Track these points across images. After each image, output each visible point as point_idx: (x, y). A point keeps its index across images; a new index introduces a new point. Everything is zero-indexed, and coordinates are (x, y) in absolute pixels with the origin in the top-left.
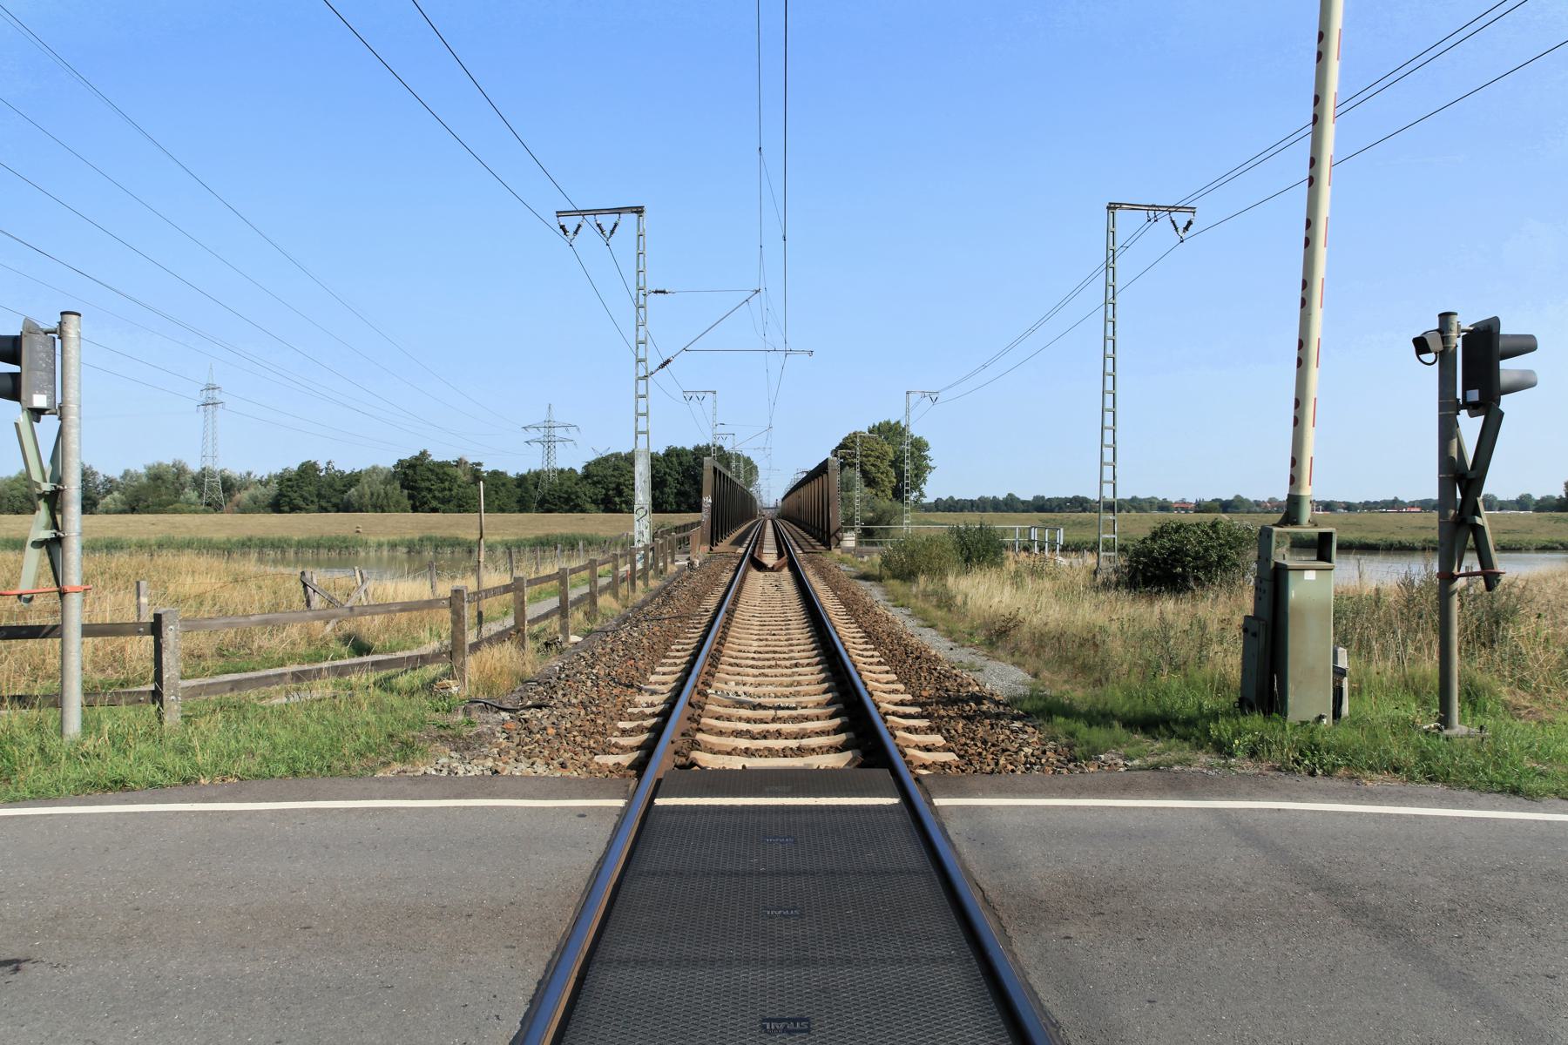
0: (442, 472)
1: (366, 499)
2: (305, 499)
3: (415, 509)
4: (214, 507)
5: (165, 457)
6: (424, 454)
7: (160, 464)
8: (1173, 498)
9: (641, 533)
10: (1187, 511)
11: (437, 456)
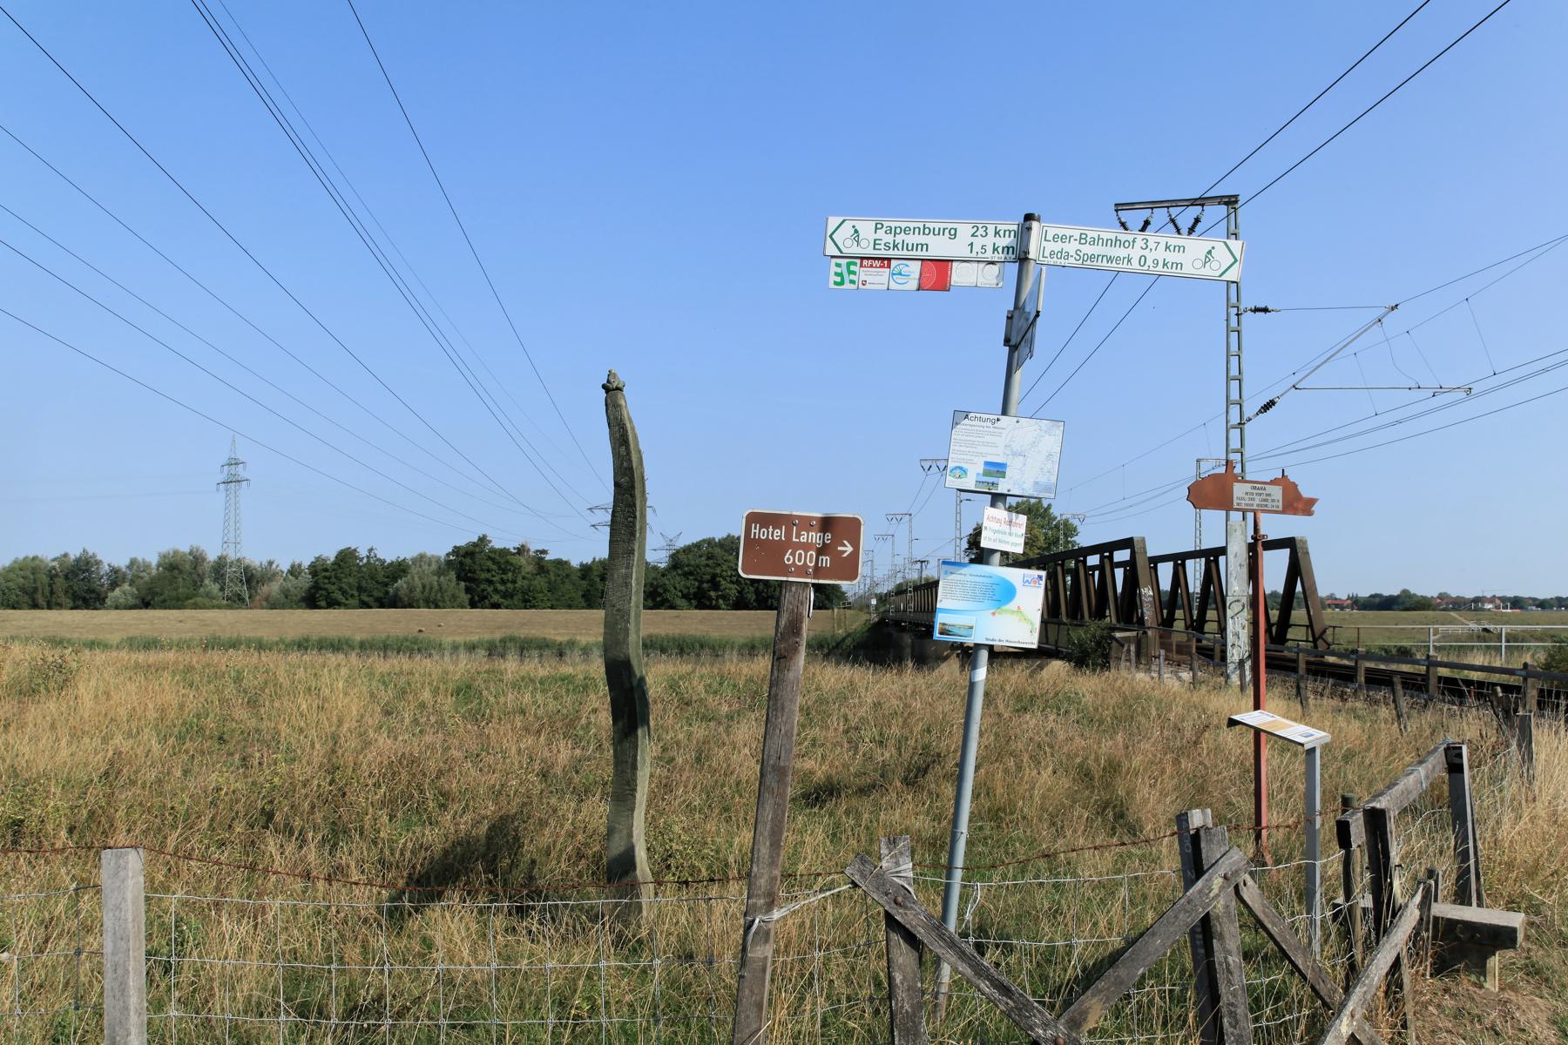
0: (503, 561)
1: (417, 594)
2: (344, 593)
3: (473, 605)
4: (236, 601)
5: (183, 545)
6: (483, 539)
7: (176, 552)
9: (1237, 635)
10: (1342, 608)
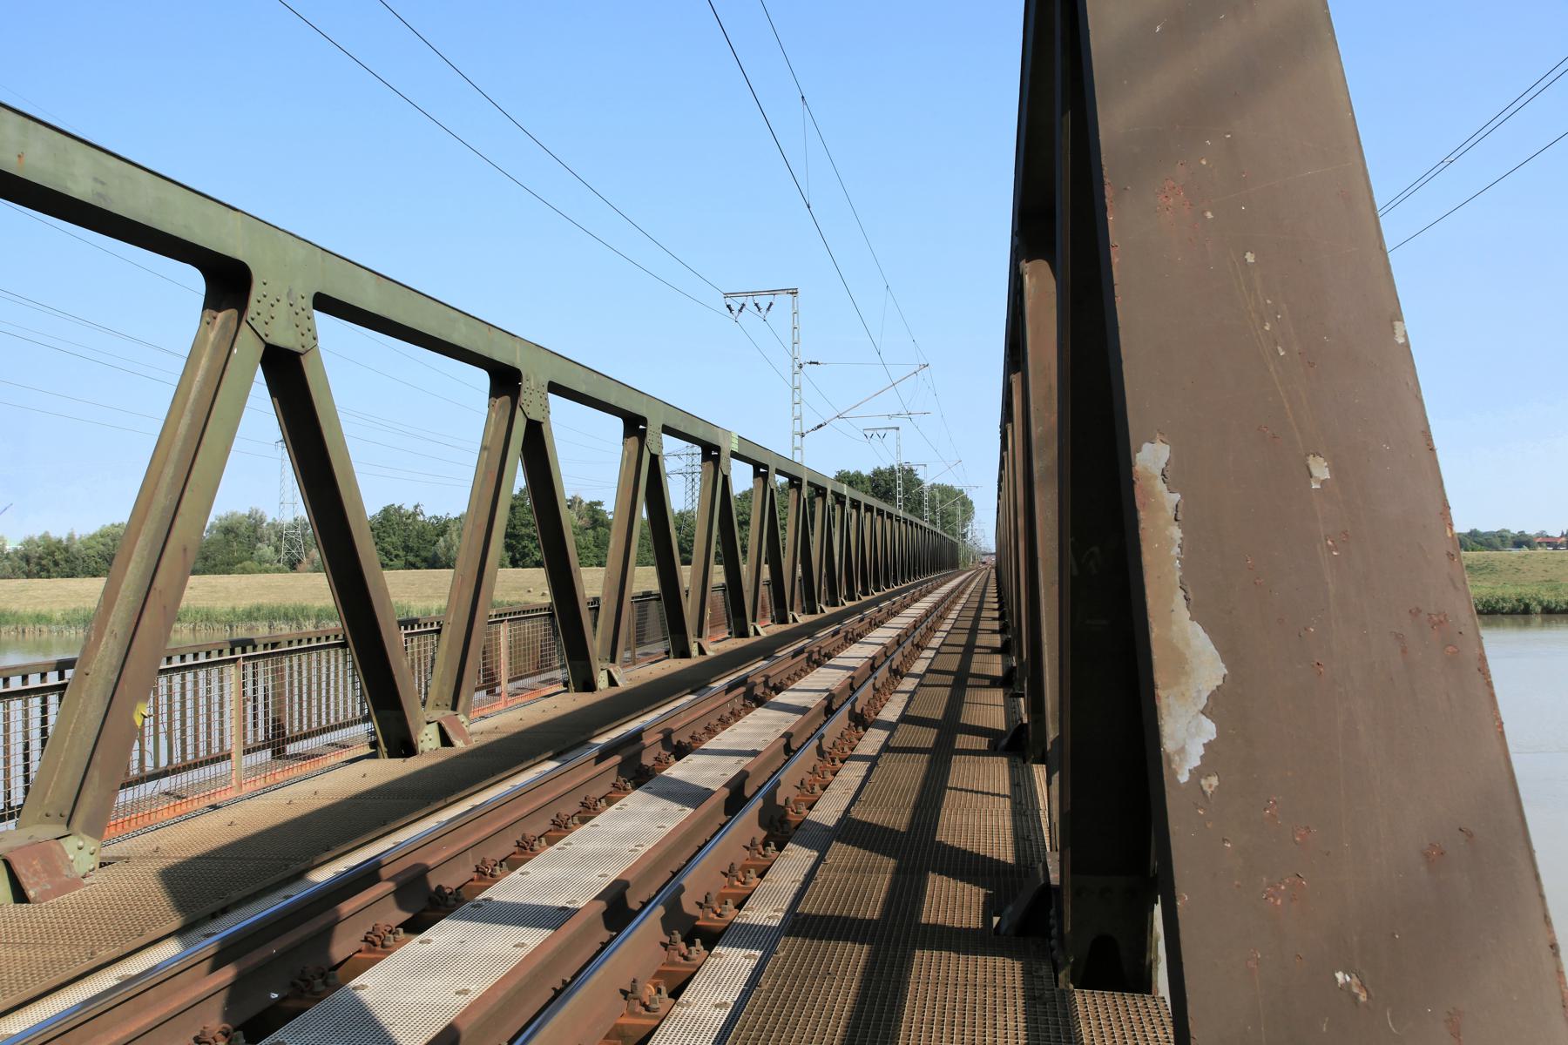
7: (233, 514)
8: (1531, 530)
11: (1482, 529)
